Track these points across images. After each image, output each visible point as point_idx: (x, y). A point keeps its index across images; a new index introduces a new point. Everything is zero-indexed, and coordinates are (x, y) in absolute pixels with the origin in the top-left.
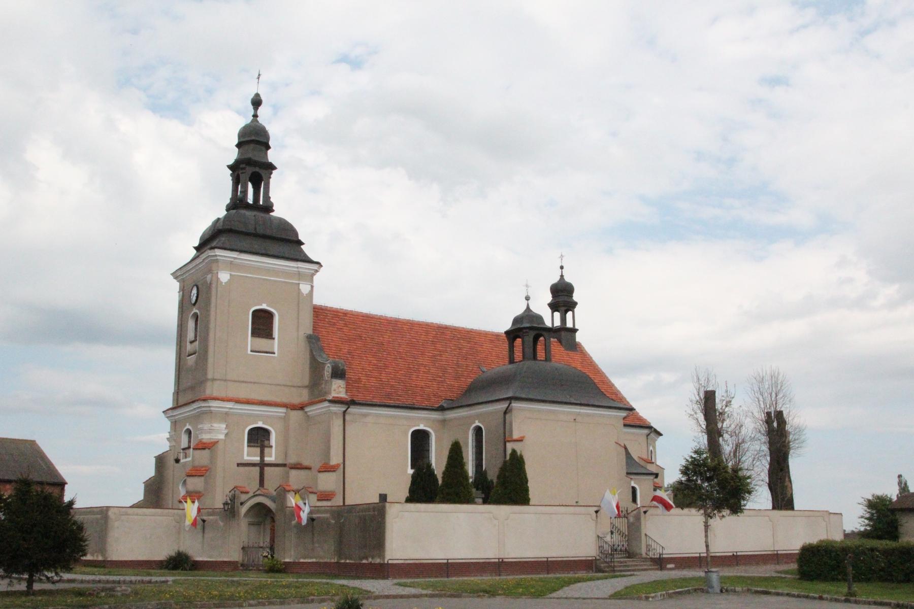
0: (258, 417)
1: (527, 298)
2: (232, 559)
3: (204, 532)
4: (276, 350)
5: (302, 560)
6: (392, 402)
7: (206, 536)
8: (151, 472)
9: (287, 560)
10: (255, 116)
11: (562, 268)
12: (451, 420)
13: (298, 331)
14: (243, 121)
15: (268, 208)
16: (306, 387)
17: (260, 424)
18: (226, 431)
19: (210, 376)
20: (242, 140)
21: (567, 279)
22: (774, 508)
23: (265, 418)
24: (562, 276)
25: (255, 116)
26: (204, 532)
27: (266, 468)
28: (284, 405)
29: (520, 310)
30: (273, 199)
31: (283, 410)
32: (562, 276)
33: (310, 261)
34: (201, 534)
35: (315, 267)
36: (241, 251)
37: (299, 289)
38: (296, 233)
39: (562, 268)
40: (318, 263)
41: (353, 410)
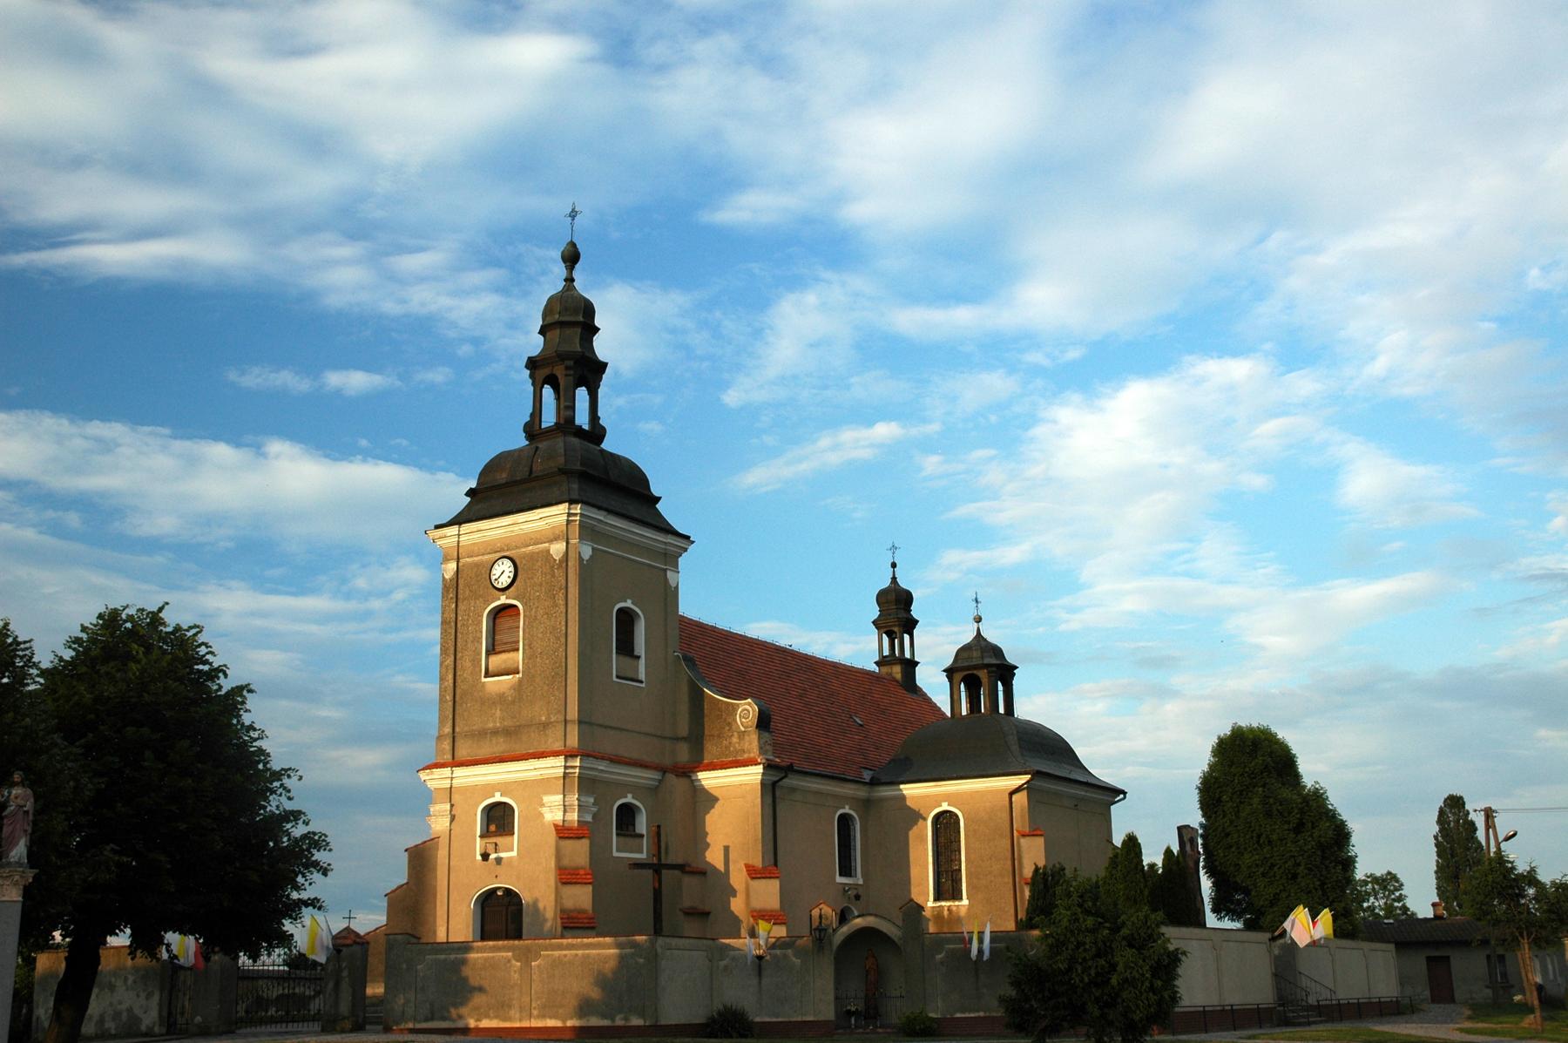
0: (489, 789)
1: (978, 620)
2: (821, 1018)
4: (642, 676)
6: (820, 770)
7: (765, 981)
9: (932, 1015)
10: (570, 280)
11: (894, 565)
15: (596, 433)
17: (498, 798)
19: (858, 647)
20: (549, 320)
23: (505, 787)
24: (894, 578)
25: (570, 280)
27: (664, 872)
28: (656, 768)
29: (968, 637)
30: (605, 420)
31: (656, 775)
32: (894, 578)
33: (669, 530)
34: (755, 981)
36: (609, 511)
38: (645, 481)
39: (894, 565)
41: (792, 781)
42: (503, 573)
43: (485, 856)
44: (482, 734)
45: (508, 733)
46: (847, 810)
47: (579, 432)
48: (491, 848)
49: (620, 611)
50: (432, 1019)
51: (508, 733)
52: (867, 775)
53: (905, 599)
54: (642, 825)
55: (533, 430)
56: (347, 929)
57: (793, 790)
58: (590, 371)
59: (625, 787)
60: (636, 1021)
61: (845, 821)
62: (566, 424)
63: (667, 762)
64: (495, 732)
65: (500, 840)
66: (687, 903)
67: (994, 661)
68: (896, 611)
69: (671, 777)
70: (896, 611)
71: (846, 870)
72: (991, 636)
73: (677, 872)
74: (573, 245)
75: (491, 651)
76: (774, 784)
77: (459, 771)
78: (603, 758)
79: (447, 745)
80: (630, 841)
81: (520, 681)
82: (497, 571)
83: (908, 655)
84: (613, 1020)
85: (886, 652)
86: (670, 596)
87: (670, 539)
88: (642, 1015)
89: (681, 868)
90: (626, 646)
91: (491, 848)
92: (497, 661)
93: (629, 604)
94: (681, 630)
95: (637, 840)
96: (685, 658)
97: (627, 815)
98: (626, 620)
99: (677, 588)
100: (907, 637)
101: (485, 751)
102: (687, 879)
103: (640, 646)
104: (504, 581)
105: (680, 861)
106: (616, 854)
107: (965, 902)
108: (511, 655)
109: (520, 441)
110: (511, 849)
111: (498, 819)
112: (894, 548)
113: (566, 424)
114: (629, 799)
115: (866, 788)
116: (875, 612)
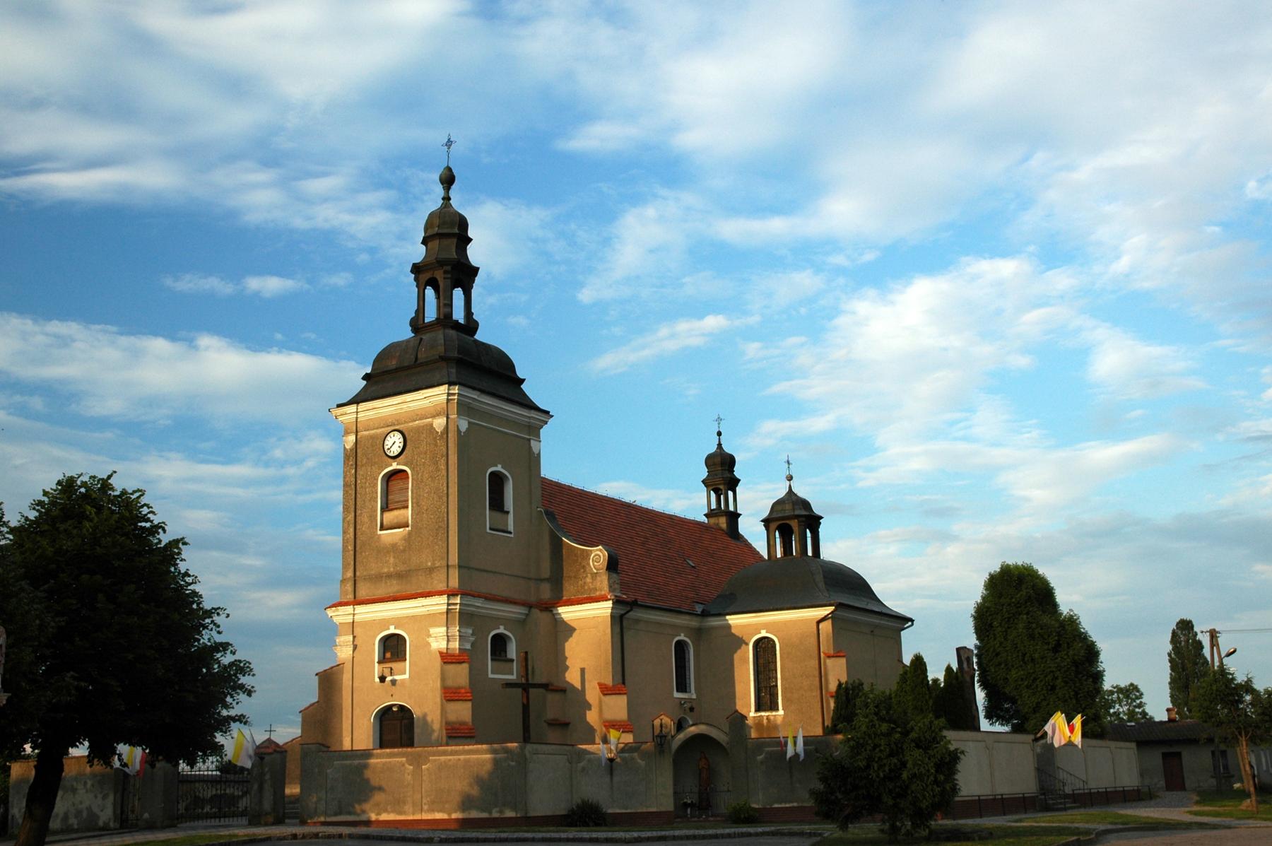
1: (790, 478)
2: (663, 809)
3: (611, 774)
4: (511, 528)
5: (776, 806)
6: (660, 604)
7: (616, 779)
8: (311, 695)
9: (754, 806)
10: (447, 199)
11: (719, 434)
12: (647, 622)
13: (531, 503)
14: (435, 204)
15: (471, 326)
16: (547, 580)
17: (392, 630)
18: (472, 639)
19: (692, 503)
20: (430, 232)
21: (727, 449)
22: (447, 723)
23: (398, 622)
24: (720, 445)
25: (447, 199)
26: (611, 774)
27: (531, 690)
28: (523, 604)
29: (782, 493)
31: (523, 610)
32: (720, 445)
33: (532, 407)
34: (607, 779)
35: (543, 417)
36: (482, 391)
37: (530, 448)
38: (510, 366)
39: (719, 434)
40: (547, 413)
42: (394, 443)
43: (382, 679)
44: (378, 578)
45: (400, 576)
46: (682, 637)
47: (456, 325)
48: (387, 672)
49: (492, 473)
50: (340, 813)
51: (400, 576)
52: (699, 609)
53: (729, 462)
54: (512, 651)
55: (417, 324)
56: (269, 740)
57: (637, 621)
58: (464, 275)
59: (498, 621)
60: (510, 814)
61: (681, 647)
62: (445, 319)
63: (533, 599)
64: (389, 576)
65: (395, 665)
66: (550, 715)
67: (804, 513)
68: (722, 473)
69: (536, 612)
70: (722, 473)
71: (682, 687)
72: (801, 492)
73: (541, 690)
74: (449, 169)
75: (386, 508)
76: (622, 617)
77: (359, 609)
78: (479, 596)
79: (349, 587)
80: (501, 665)
81: (410, 533)
82: (389, 442)
83: (731, 508)
84: (490, 813)
85: (714, 506)
86: (534, 461)
87: (533, 414)
88: (514, 808)
89: (545, 686)
90: (497, 503)
91: (387, 672)
92: (390, 517)
93: (499, 468)
94: (543, 489)
95: (509, 664)
96: (547, 513)
97: (499, 643)
98: (497, 482)
99: (539, 454)
100: (730, 494)
101: (381, 591)
102: (551, 697)
103: (509, 503)
104: (396, 450)
105: (544, 681)
106: (491, 676)
107: (781, 712)
108: (402, 511)
109: (406, 334)
110: (403, 673)
111: (393, 647)
112: (719, 420)
113: (445, 319)
114: (501, 630)
115: (699, 619)
116: (704, 473)
